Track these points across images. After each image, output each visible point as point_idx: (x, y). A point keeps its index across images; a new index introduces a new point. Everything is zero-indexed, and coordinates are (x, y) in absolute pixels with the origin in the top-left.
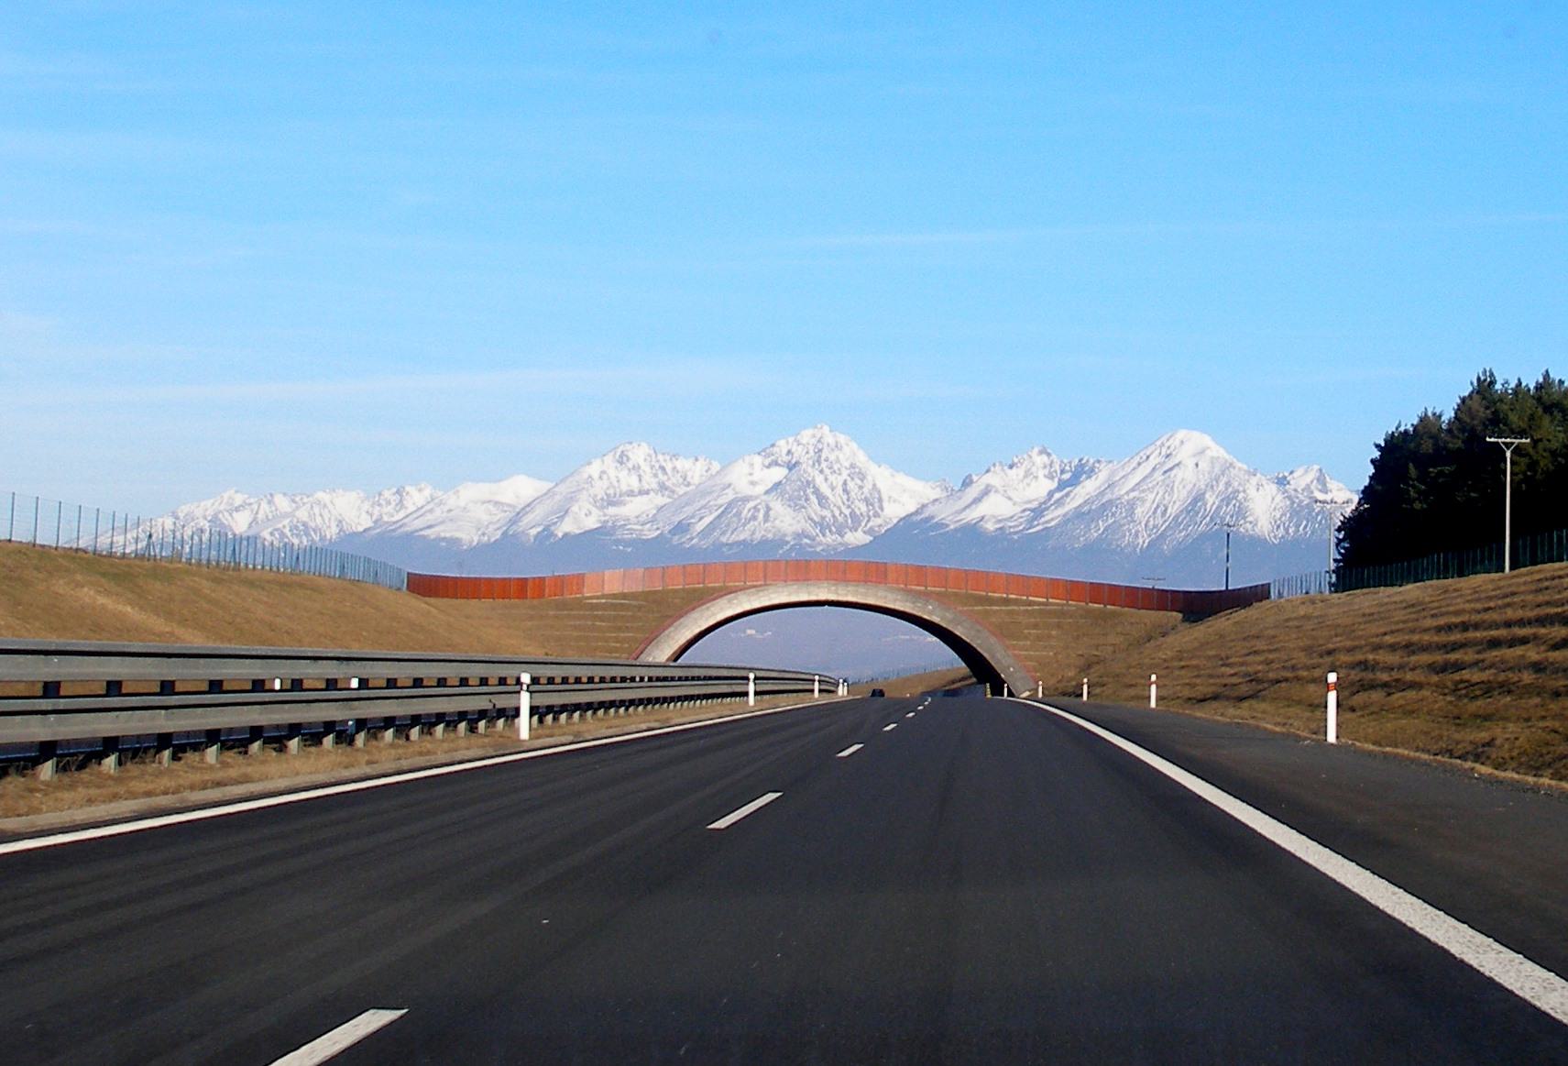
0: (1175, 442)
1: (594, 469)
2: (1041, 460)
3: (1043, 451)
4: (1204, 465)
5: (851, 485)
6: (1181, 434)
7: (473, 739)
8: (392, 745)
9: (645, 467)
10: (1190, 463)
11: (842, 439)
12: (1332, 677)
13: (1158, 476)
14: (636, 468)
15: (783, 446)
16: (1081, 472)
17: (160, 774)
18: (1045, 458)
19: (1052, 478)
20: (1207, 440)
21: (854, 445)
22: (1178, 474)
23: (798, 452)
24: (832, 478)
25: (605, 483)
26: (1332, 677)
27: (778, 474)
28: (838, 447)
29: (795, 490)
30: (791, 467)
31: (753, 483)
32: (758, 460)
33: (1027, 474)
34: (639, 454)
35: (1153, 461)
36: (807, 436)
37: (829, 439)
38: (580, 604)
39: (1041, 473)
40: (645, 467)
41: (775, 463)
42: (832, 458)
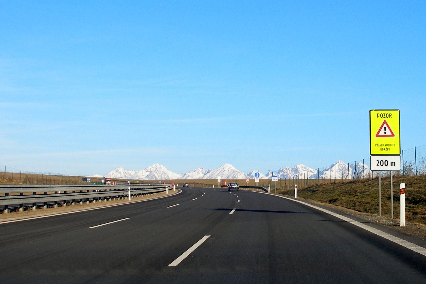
0: (225, 166)
1: (111, 173)
2: (201, 170)
3: (201, 168)
4: (230, 171)
5: (162, 175)
6: (226, 164)
7: (121, 201)
8: (95, 204)
9: (122, 173)
10: (227, 170)
11: (162, 166)
12: (296, 185)
13: (221, 173)
14: (120, 173)
15: (149, 168)
16: (209, 172)
17: (105, 203)
18: (202, 169)
19: (203, 173)
20: (231, 166)
21: (164, 167)
22: (225, 173)
23: (152, 169)
24: (158, 174)
25: (113, 176)
26: (296, 185)
27: (148, 173)
28: (160, 168)
29: (125, 176)
30: (150, 172)
31: (143, 175)
32: (144, 171)
33: (198, 173)
34: (121, 170)
35: (220, 170)
36: (154, 166)
37: (159, 166)
38: (373, 179)
39: (201, 172)
40: (122, 173)
41: (147, 171)
42: (159, 170)
